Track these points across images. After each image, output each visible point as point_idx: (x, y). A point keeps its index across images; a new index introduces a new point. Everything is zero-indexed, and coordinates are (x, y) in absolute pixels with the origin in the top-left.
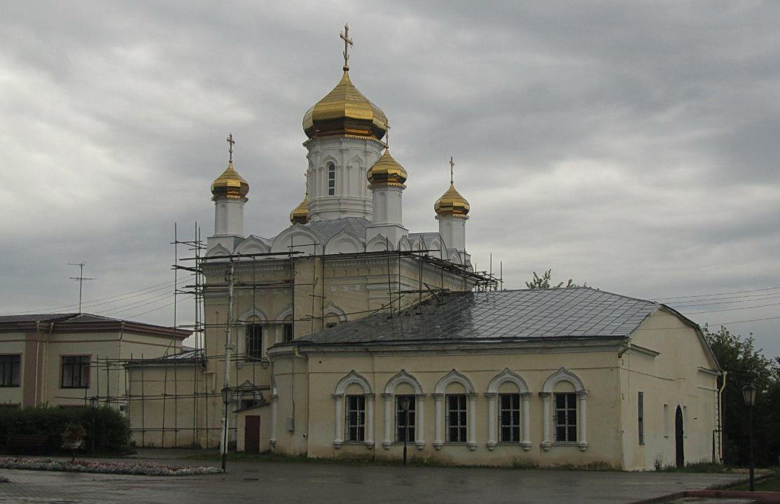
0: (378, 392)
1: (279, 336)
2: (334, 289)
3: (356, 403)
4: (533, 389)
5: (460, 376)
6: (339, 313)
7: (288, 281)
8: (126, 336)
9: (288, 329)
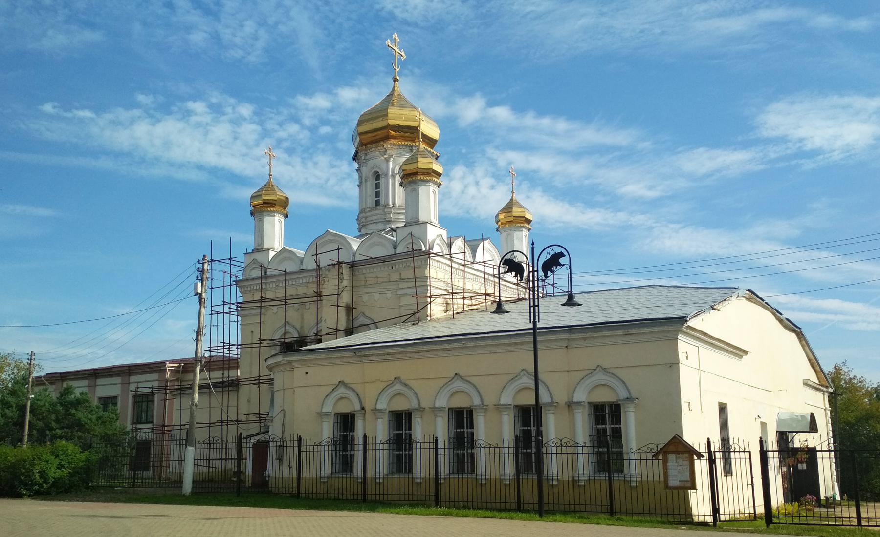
0: (490, 400)
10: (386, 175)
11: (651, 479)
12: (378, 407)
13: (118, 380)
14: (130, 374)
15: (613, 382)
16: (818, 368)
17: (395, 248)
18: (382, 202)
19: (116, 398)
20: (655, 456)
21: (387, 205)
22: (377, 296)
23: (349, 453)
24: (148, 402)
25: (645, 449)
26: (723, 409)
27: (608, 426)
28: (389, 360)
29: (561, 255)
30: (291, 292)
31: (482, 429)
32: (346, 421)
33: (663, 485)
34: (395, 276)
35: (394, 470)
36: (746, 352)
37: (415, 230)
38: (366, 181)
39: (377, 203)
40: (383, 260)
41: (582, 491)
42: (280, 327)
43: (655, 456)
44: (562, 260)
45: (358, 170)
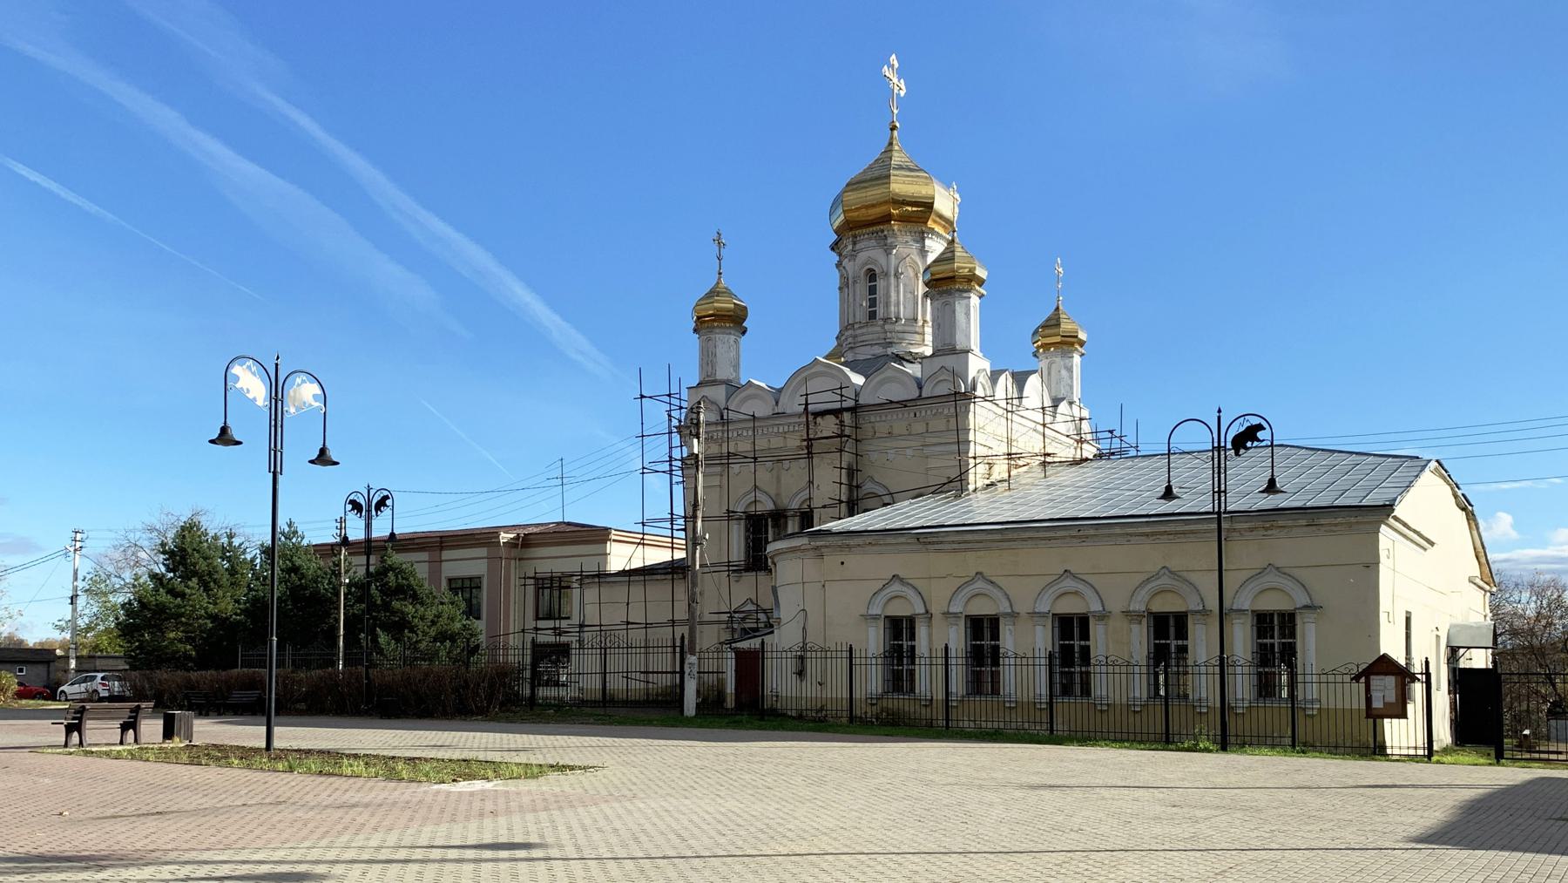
0: (1022, 608)
6: (881, 491)
10: (887, 275)
11: (1332, 706)
12: (952, 610)
14: (442, 548)
16: (1483, 560)
17: (920, 388)
18: (880, 312)
20: (1357, 678)
21: (886, 320)
23: (987, 643)
24: (561, 588)
25: (1342, 670)
27: (1276, 641)
28: (966, 550)
29: (1260, 427)
30: (762, 444)
31: (1100, 641)
32: (900, 629)
33: (1364, 714)
34: (919, 427)
35: (1443, 733)
36: (1432, 544)
37: (949, 361)
38: (855, 282)
39: (873, 315)
40: (903, 404)
41: (1240, 722)
42: (749, 493)
43: (1357, 678)
44: (1260, 435)
45: (839, 265)
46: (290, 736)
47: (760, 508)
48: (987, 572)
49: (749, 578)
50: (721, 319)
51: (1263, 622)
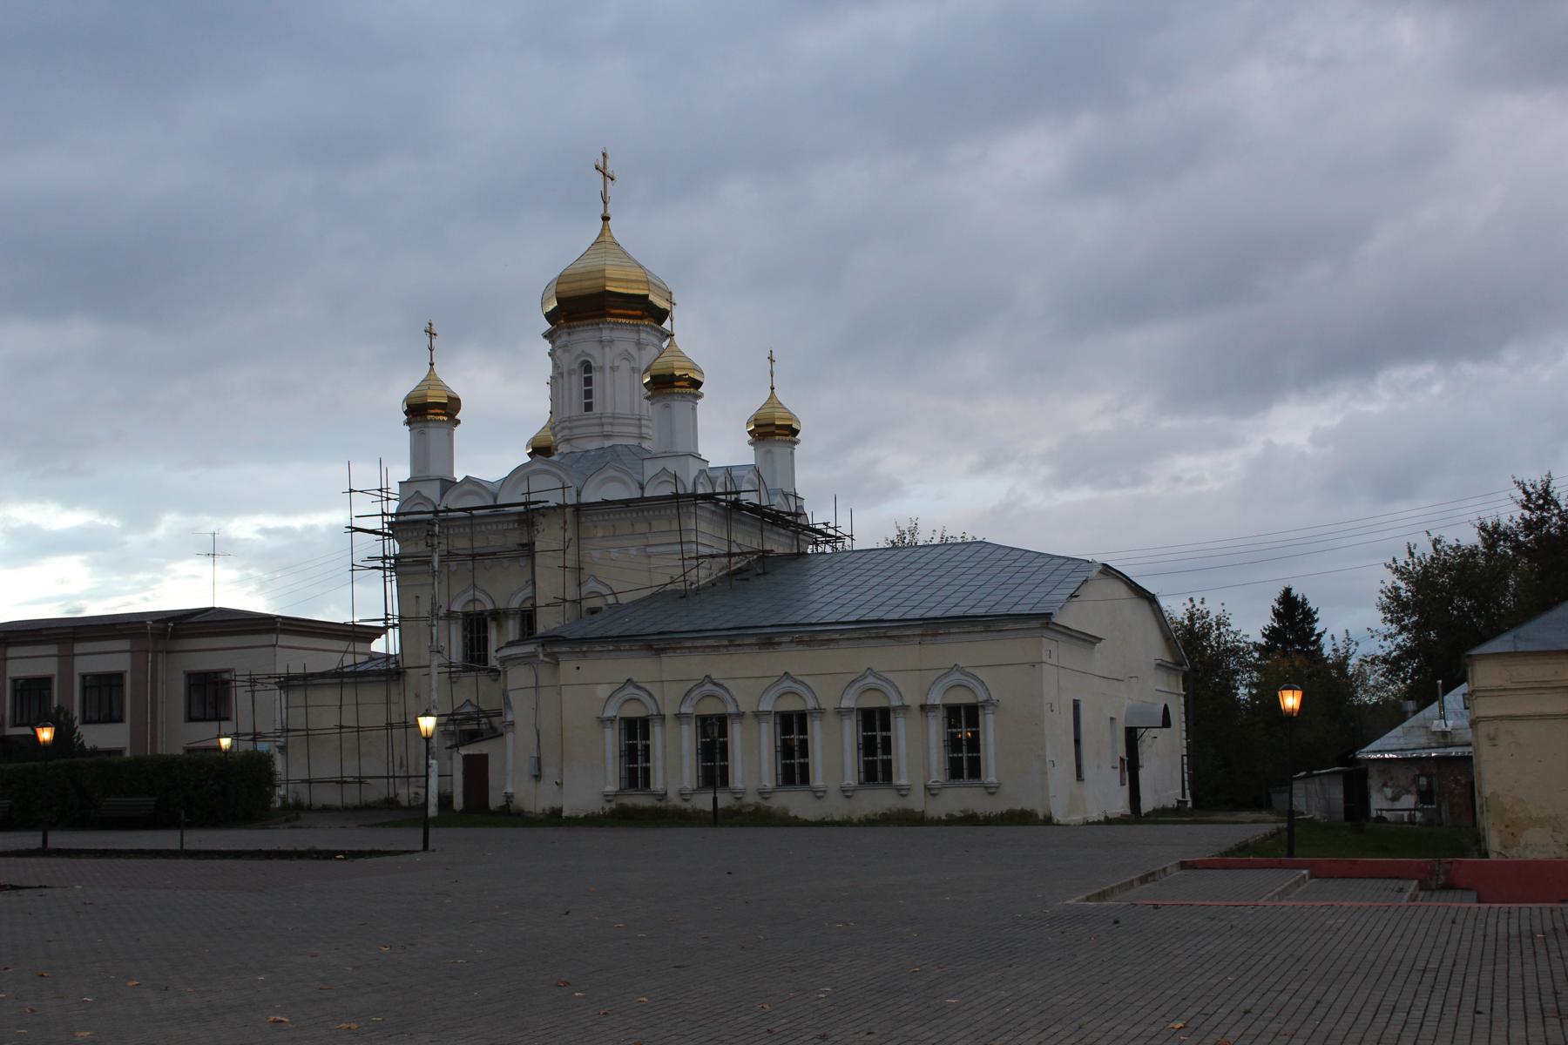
0: (669, 711)
1: (512, 629)
2: (596, 554)
3: (636, 731)
4: (828, 703)
5: (639, 688)
6: (605, 591)
7: (523, 545)
8: (284, 640)
9: (528, 618)
10: (602, 368)
13: (53, 649)
15: (972, 683)
19: (119, 676)
22: (614, 554)
23: (796, 737)
26: (1076, 705)
46: (57, 839)
47: (479, 608)
48: (876, 668)
49: (468, 680)
50: (430, 413)
51: (705, 722)
